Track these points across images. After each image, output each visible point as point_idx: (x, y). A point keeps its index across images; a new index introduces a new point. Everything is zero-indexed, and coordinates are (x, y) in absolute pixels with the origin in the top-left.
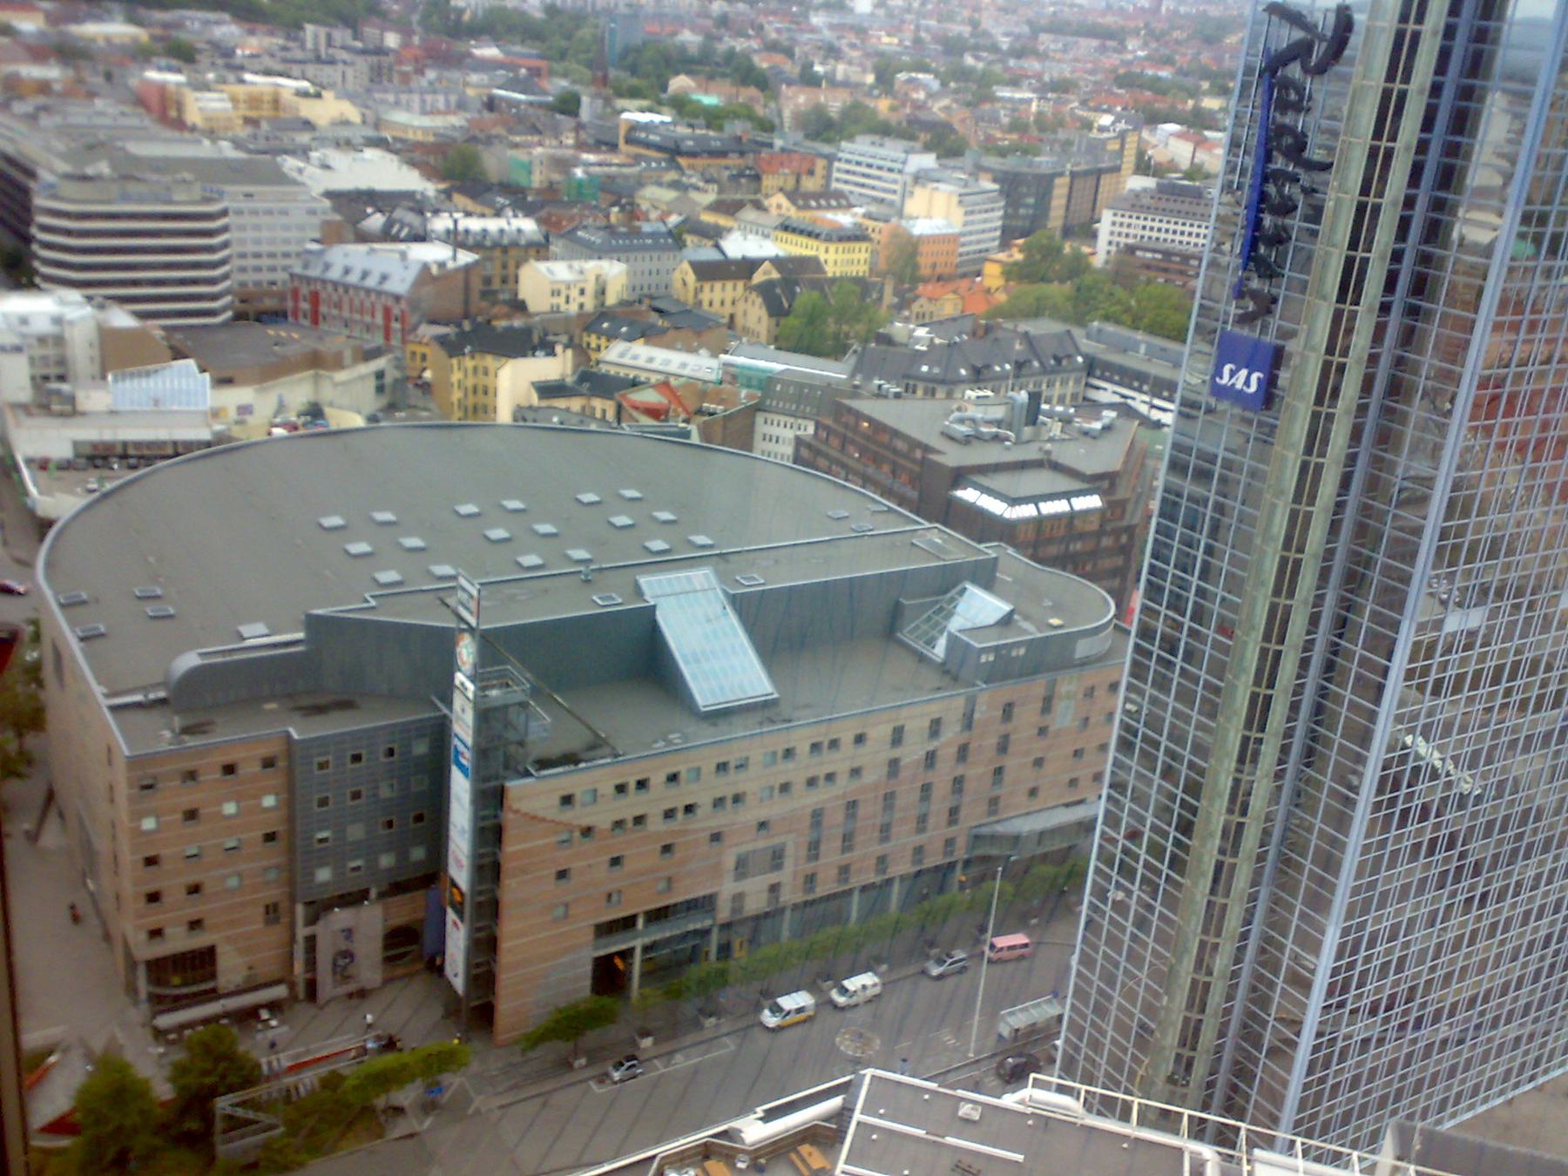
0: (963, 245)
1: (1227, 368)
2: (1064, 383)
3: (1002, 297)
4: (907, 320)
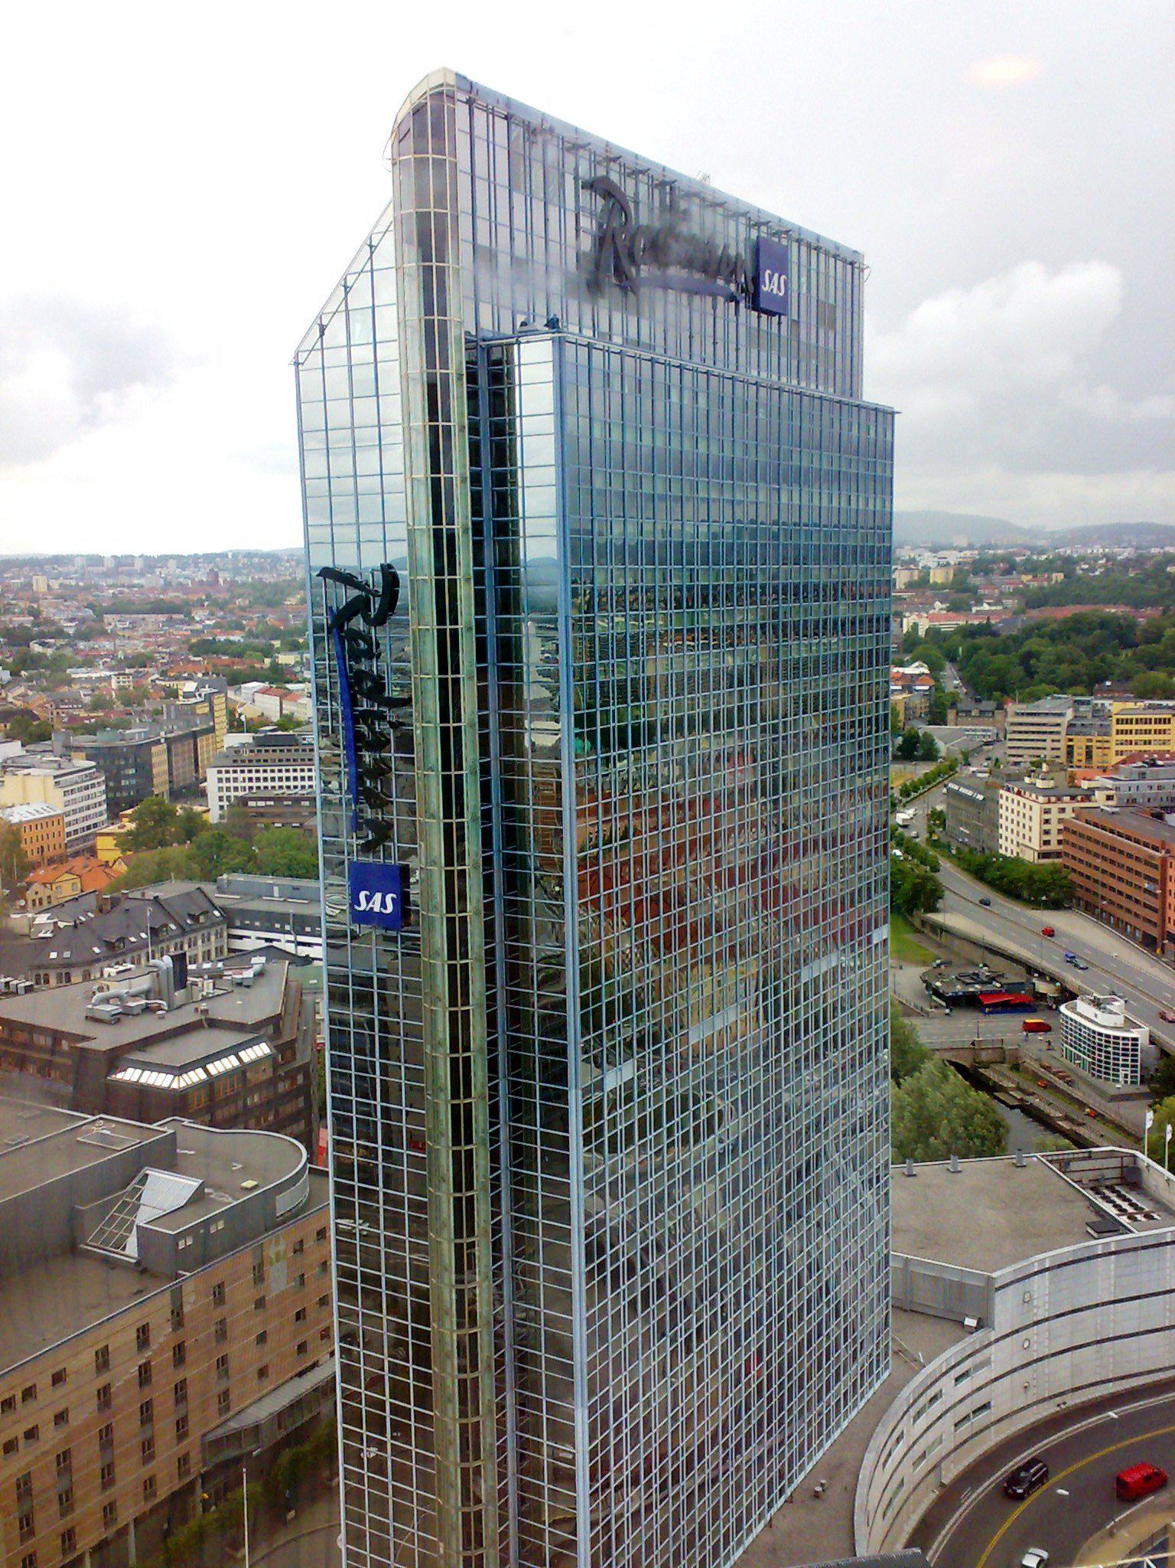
0: (69, 824)
1: (362, 895)
2: (206, 939)
3: (122, 868)
4: (23, 909)
